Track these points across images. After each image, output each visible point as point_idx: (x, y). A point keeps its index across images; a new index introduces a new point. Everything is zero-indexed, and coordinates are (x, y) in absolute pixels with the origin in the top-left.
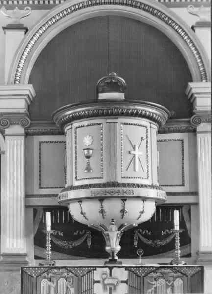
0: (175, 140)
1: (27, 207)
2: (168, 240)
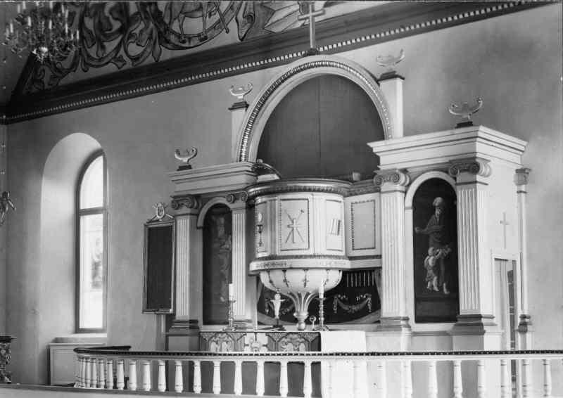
0: (364, 202)
2: (362, 305)
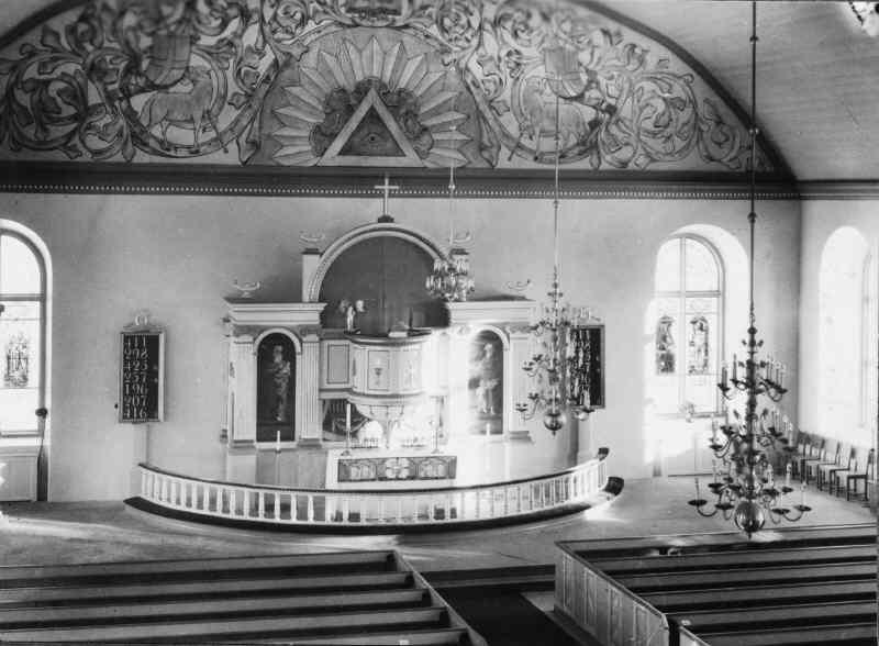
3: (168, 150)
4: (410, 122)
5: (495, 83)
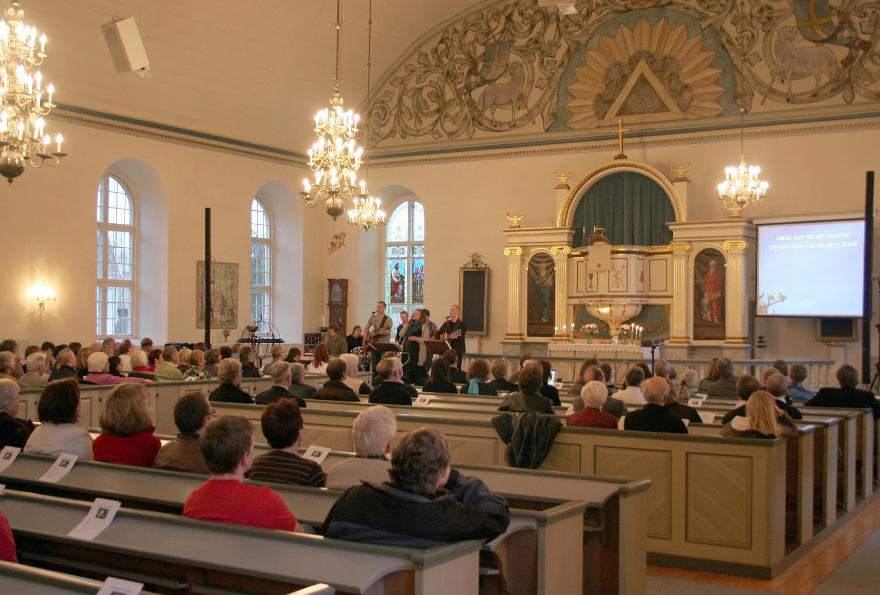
1: (568, 305)
3: (495, 126)
4: (673, 82)
5: (748, 38)
